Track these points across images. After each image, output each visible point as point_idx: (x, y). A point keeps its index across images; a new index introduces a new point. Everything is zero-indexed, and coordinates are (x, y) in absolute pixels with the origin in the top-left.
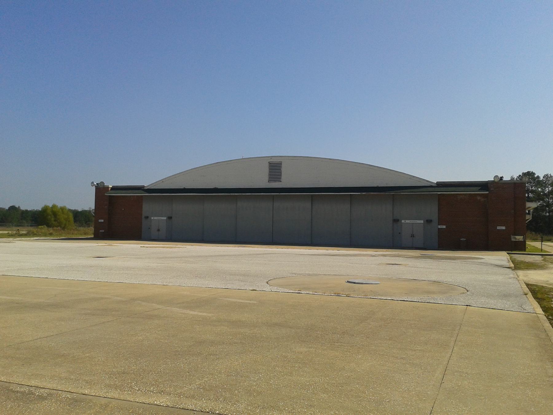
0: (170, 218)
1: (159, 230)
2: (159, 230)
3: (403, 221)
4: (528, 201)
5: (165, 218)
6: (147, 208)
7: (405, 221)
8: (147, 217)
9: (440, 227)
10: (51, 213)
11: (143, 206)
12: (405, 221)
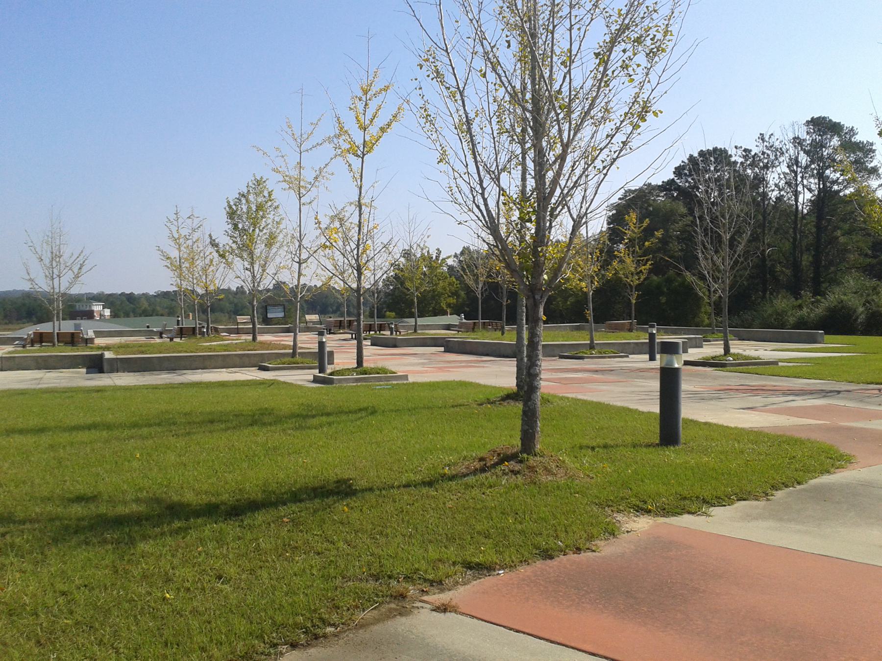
9: (191, 318)
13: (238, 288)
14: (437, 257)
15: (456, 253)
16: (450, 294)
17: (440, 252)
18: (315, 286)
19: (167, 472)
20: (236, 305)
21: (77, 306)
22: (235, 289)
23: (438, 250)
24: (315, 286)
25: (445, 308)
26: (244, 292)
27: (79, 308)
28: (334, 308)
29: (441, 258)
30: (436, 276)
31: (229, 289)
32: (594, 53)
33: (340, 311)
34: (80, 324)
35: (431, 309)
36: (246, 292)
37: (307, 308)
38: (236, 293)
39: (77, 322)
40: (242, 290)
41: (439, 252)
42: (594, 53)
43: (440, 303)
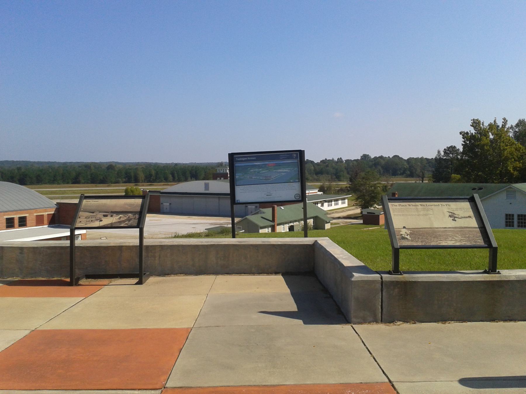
0: (170, 204)
1: (167, 209)
2: (167, 209)
3: (248, 207)
4: (326, 224)
5: (168, 204)
6: (162, 200)
7: (207, 186)
8: (162, 203)
10: (130, 191)
11: (161, 198)
12: (207, 186)
13: (338, 159)
14: (504, 126)
15: (512, 126)
16: (517, 159)
17: (507, 121)
18: (389, 157)
19: (478, 142)
20: (337, 170)
21: (218, 170)
22: (336, 160)
23: (504, 119)
24: (389, 157)
25: (512, 171)
26: (342, 161)
27: (219, 171)
28: (402, 172)
29: (507, 126)
30: (503, 142)
31: (333, 159)
32: (462, 144)
33: (405, 173)
34: (209, 183)
35: (498, 172)
36: (343, 161)
37: (383, 171)
38: (337, 162)
39: (207, 181)
40: (340, 160)
41: (505, 121)
42: (462, 144)
43: (506, 167)
